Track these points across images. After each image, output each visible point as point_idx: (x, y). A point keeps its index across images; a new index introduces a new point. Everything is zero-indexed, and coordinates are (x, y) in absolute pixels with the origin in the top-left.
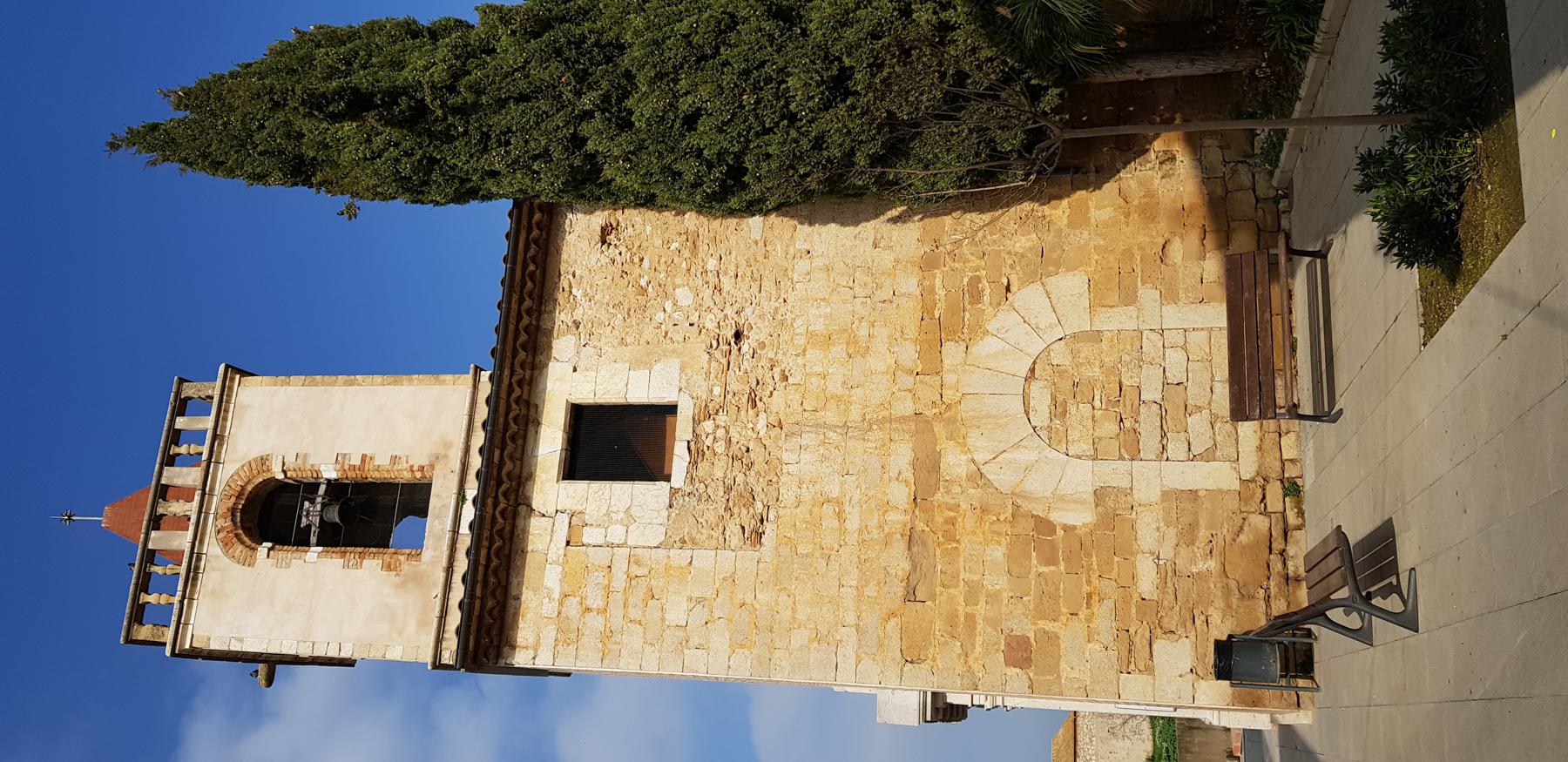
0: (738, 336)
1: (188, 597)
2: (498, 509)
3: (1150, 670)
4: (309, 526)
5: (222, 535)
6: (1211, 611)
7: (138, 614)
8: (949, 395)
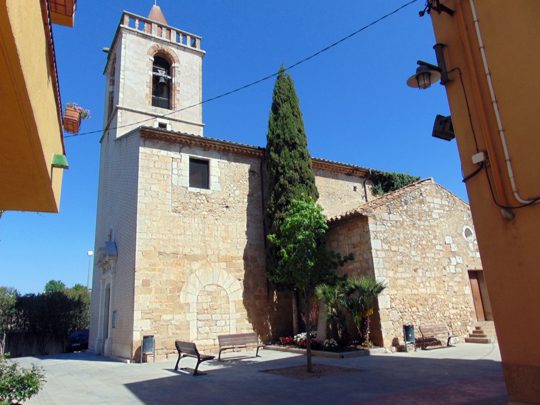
0: (227, 207)
1: (138, 34)
2: (182, 139)
3: (143, 318)
4: (158, 72)
5: (157, 46)
6: (158, 335)
7: (132, 17)
8: (212, 264)
